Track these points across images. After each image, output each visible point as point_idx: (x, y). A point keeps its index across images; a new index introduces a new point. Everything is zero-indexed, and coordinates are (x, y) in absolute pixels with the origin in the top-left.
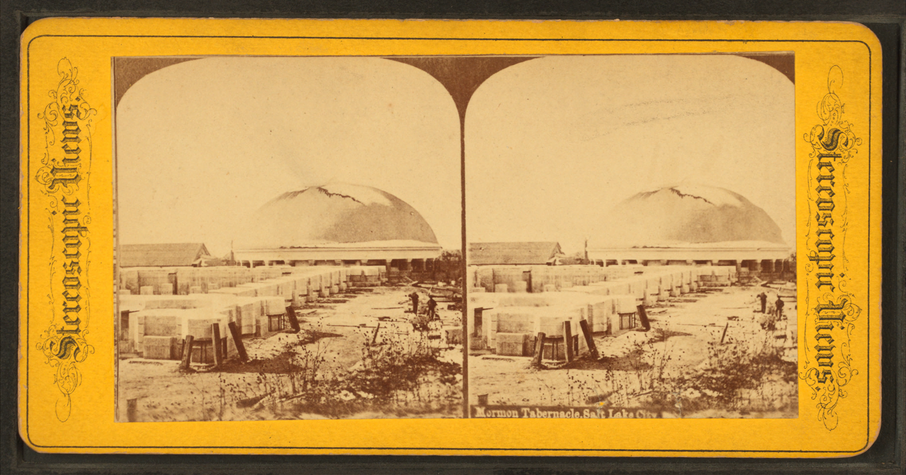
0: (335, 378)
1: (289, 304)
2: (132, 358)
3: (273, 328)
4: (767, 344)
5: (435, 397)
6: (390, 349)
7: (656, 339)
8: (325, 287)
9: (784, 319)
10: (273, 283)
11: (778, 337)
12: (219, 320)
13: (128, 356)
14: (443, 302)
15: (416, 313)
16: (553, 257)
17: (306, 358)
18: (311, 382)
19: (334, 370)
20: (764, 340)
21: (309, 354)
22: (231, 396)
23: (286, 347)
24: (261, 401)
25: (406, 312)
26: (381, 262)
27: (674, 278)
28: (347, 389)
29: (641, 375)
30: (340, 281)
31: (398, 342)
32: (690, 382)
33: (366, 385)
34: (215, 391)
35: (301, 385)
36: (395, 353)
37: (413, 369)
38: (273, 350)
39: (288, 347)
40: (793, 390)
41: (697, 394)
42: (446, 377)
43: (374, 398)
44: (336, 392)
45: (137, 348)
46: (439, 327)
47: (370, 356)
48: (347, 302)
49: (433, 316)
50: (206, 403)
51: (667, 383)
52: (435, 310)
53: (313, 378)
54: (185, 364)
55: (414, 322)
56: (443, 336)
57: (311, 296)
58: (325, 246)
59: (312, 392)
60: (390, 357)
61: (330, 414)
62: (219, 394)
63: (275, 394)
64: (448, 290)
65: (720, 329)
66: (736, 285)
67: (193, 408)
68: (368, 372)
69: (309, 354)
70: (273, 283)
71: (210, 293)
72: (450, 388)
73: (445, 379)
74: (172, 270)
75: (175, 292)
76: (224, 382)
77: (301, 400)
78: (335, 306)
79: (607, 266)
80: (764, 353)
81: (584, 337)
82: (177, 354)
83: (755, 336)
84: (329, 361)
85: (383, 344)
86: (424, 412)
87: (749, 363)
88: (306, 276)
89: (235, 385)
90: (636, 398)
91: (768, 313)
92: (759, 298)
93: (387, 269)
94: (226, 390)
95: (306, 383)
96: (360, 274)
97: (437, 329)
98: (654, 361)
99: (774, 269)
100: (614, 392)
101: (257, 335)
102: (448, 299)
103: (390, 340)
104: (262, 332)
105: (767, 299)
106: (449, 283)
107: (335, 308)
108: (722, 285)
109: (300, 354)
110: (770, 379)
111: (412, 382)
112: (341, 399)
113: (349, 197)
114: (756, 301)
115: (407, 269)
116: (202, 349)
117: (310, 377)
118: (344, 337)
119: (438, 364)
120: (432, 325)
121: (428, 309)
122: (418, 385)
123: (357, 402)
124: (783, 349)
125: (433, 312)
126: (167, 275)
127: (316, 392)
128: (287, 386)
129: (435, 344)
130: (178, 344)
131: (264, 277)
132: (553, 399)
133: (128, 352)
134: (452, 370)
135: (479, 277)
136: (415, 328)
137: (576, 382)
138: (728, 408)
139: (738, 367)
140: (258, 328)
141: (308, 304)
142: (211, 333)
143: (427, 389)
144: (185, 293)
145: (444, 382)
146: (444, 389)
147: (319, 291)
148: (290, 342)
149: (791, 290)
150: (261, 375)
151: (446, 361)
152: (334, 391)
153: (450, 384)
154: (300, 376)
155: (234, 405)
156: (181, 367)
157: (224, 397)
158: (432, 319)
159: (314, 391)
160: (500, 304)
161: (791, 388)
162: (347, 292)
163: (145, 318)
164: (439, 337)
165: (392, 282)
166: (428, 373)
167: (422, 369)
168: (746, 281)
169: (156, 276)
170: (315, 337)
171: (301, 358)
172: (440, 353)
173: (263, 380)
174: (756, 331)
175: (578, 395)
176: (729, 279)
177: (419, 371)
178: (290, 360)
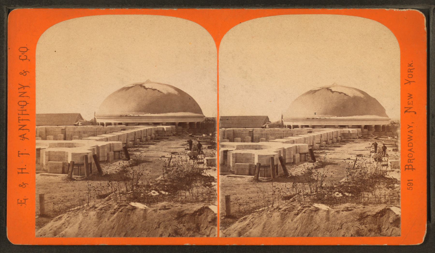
1: (125, 145)
2: (229, 174)
3: (302, 160)
4: (378, 169)
5: (201, 194)
6: (177, 169)
7: (319, 166)
9: (387, 156)
10: (302, 137)
11: (383, 165)
12: (274, 155)
14: (390, 147)
15: (191, 150)
17: (133, 173)
18: (136, 186)
19: (148, 180)
20: (376, 167)
22: (94, 192)
24: (110, 196)
25: (186, 150)
26: (359, 127)
27: (328, 135)
28: (154, 190)
29: (127, 183)
30: (151, 133)
31: (181, 165)
32: (337, 189)
33: (165, 187)
34: (85, 190)
35: (130, 188)
37: (189, 179)
38: (302, 171)
39: (124, 167)
41: (157, 193)
42: (207, 184)
43: (169, 194)
44: (149, 191)
45: (45, 168)
46: (203, 158)
47: (167, 173)
48: (341, 147)
49: (200, 152)
50: (81, 197)
52: (201, 148)
53: (321, 185)
54: (256, 178)
55: (190, 155)
56: (205, 162)
57: (322, 144)
58: (330, 118)
59: (320, 193)
60: (177, 173)
61: (146, 202)
62: (88, 192)
63: (301, 194)
64: (208, 138)
65: (352, 161)
66: (176, 136)
67: (74, 199)
68: (165, 181)
69: (135, 171)
70: (302, 137)
71: (270, 141)
72: (209, 189)
73: (206, 184)
74: (63, 127)
75: (65, 139)
76: (90, 186)
77: (314, 196)
78: (335, 149)
80: (376, 174)
81: (281, 165)
83: (371, 165)
84: (145, 175)
85: (174, 166)
86: (377, 204)
88: (319, 133)
89: (96, 187)
91: (378, 153)
92: (374, 145)
93: (176, 127)
94: (91, 190)
95: (133, 186)
96: (348, 133)
97: (202, 158)
98: (318, 178)
99: (381, 130)
100: (297, 194)
101: (108, 161)
102: (207, 143)
103: (177, 164)
104: (110, 160)
105: (378, 145)
106: (208, 135)
107: (335, 150)
108: (354, 138)
109: (130, 171)
110: (379, 186)
111: (189, 186)
113: (343, 93)
114: (372, 147)
116: (265, 170)
117: (319, 185)
118: (338, 165)
119: (202, 177)
120: (200, 157)
121: (197, 148)
122: (375, 189)
123: (160, 196)
124: (386, 171)
125: (200, 150)
126: (248, 132)
127: (138, 191)
128: (123, 188)
129: (201, 166)
131: (112, 131)
132: (265, 198)
133: (40, 170)
134: (393, 182)
136: (191, 158)
137: (277, 189)
139: (362, 181)
140: (108, 158)
141: (135, 144)
142: (84, 159)
143: (197, 190)
145: (388, 188)
146: (388, 191)
147: (140, 139)
148: (125, 165)
149: (206, 138)
151: (206, 175)
152: (148, 191)
153: (391, 189)
155: (96, 198)
156: (68, 178)
157: (90, 193)
158: (199, 154)
161: (390, 192)
162: (341, 142)
163: (49, 152)
164: (203, 163)
165: (364, 137)
166: (197, 181)
167: (194, 179)
168: (366, 136)
169: (55, 130)
170: (137, 162)
171: (131, 173)
173: (110, 185)
175: (278, 195)
177: (192, 180)
178: (125, 174)
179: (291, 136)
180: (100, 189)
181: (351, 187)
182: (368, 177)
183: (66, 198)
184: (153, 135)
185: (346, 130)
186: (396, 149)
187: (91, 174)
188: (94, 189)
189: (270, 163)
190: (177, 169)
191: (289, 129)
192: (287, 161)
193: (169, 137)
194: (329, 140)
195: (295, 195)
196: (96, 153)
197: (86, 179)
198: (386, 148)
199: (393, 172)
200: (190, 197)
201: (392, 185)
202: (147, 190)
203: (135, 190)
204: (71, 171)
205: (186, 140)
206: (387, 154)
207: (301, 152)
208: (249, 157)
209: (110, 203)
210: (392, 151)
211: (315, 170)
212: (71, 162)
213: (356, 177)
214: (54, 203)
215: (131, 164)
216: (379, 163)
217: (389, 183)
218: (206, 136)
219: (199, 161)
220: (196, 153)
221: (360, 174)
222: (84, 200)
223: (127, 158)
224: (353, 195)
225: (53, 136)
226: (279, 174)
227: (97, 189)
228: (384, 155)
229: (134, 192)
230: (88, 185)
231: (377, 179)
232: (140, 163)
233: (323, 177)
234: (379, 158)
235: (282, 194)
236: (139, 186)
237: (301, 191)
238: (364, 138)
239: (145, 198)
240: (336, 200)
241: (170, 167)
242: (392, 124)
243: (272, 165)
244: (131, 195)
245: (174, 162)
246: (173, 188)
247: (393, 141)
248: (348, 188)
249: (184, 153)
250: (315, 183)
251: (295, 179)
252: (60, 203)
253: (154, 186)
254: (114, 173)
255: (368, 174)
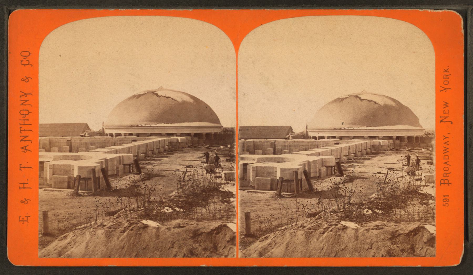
0: (161, 200)
1: (135, 158)
2: (249, 189)
3: (328, 174)
4: (411, 183)
5: (218, 211)
6: (193, 183)
8: (359, 151)
9: (420, 170)
10: (329, 148)
11: (417, 180)
13: (44, 187)
15: (207, 163)
16: (84, 132)
19: (161, 196)
20: (408, 181)
21: (147, 186)
22: (102, 209)
23: (133, 182)
24: (119, 213)
25: (202, 163)
26: (390, 138)
28: (168, 206)
29: (138, 199)
30: (164, 145)
31: (197, 180)
32: (366, 205)
35: (142, 204)
36: (195, 186)
37: (206, 195)
38: (328, 186)
39: (135, 182)
40: (425, 209)
41: (171, 210)
42: (225, 199)
43: (184, 211)
44: (162, 208)
46: (221, 171)
47: (181, 188)
48: (371, 160)
49: (217, 165)
50: (88, 214)
51: (353, 206)
52: (219, 161)
53: (349, 201)
54: (278, 193)
55: (206, 169)
56: (223, 176)
58: (359, 128)
59: (148, 208)
60: (193, 188)
63: (327, 211)
64: (226, 150)
65: (383, 175)
66: (191, 148)
68: (180, 197)
69: (147, 186)
70: (329, 148)
71: (294, 154)
73: (224, 200)
74: (69, 138)
75: (70, 151)
76: (98, 202)
77: (342, 214)
78: (364, 162)
79: (116, 137)
80: (409, 189)
82: (274, 188)
83: (404, 179)
84: (158, 190)
87: (400, 194)
88: (347, 145)
89: (104, 204)
90: (336, 214)
91: (411, 166)
92: (406, 158)
93: (393, 141)
94: (99, 206)
95: (144, 202)
97: (220, 172)
98: (346, 193)
99: (415, 142)
100: (323, 211)
105: (411, 158)
106: (227, 146)
108: (385, 150)
109: (142, 186)
110: (412, 203)
111: (205, 202)
112: (165, 212)
113: (373, 101)
114: (404, 159)
115: (404, 142)
116: (288, 184)
117: (347, 201)
120: (217, 170)
121: (214, 161)
122: (208, 204)
123: (173, 213)
124: (420, 186)
125: (218, 163)
127: (150, 208)
128: (134, 204)
129: (218, 181)
130: (72, 180)
132: (288, 215)
135: (246, 145)
136: (207, 172)
137: (301, 205)
138: (189, 218)
139: (394, 197)
140: (118, 171)
141: (147, 157)
142: (91, 173)
143: (214, 206)
144: (76, 151)
145: (422, 205)
146: (422, 208)
148: (135, 179)
149: (223, 150)
150: (119, 198)
151: (224, 190)
152: (161, 207)
153: (425, 206)
154: (141, 199)
155: (104, 216)
156: (74, 193)
158: (217, 167)
159: (149, 207)
160: (54, 159)
162: (371, 154)
163: (53, 165)
164: (220, 177)
165: (396, 149)
166: (214, 197)
167: (211, 195)
168: (398, 148)
170: (149, 176)
172: (420, 188)
173: (120, 201)
174: (404, 176)
175: (302, 212)
176: (389, 147)
177: (209, 196)
178: (136, 190)
179: (316, 148)
180: (109, 205)
181: (382, 203)
182: (401, 193)
183: (72, 215)
184: (166, 147)
185: (376, 141)
186: (430, 162)
187: (99, 189)
188: (102, 206)
189: (294, 178)
190: (193, 183)
191: (314, 140)
192: (312, 175)
193: (184, 149)
194: (357, 152)
195: (321, 212)
196: (104, 167)
197: (94, 195)
198: (420, 161)
199: (428, 187)
200: (207, 214)
201: (426, 201)
202: (160, 206)
203: (147, 206)
204: (77, 186)
205: (203, 153)
206: (421, 168)
207: (327, 165)
208: (270, 170)
209: (120, 221)
210: (426, 164)
211: (342, 185)
212: (77, 176)
213: (387, 192)
214: (58, 221)
215: (142, 178)
216: (412, 177)
217: (423, 199)
218: (224, 148)
219: (216, 175)
220: (213, 166)
221: (392, 189)
222: (91, 218)
223: (138, 172)
224: (384, 212)
225: (57, 148)
226: (303, 189)
227: (106, 205)
228: (418, 168)
229: (346, 211)
230: (95, 201)
231: (410, 194)
232: (152, 177)
233: (351, 192)
234: (413, 171)
235: (306, 210)
236: (151, 202)
237: (328, 208)
238: (396, 151)
239: (158, 216)
240: (366, 217)
241: (185, 181)
242: (426, 135)
243: (296, 180)
244: (143, 212)
245: (189, 176)
246: (187, 204)
247: (427, 153)
248: (379, 204)
249: (200, 166)
250: (342, 199)
251: (320, 195)
252: (65, 221)
253: (167, 202)
254: (124, 188)
255: (400, 189)
